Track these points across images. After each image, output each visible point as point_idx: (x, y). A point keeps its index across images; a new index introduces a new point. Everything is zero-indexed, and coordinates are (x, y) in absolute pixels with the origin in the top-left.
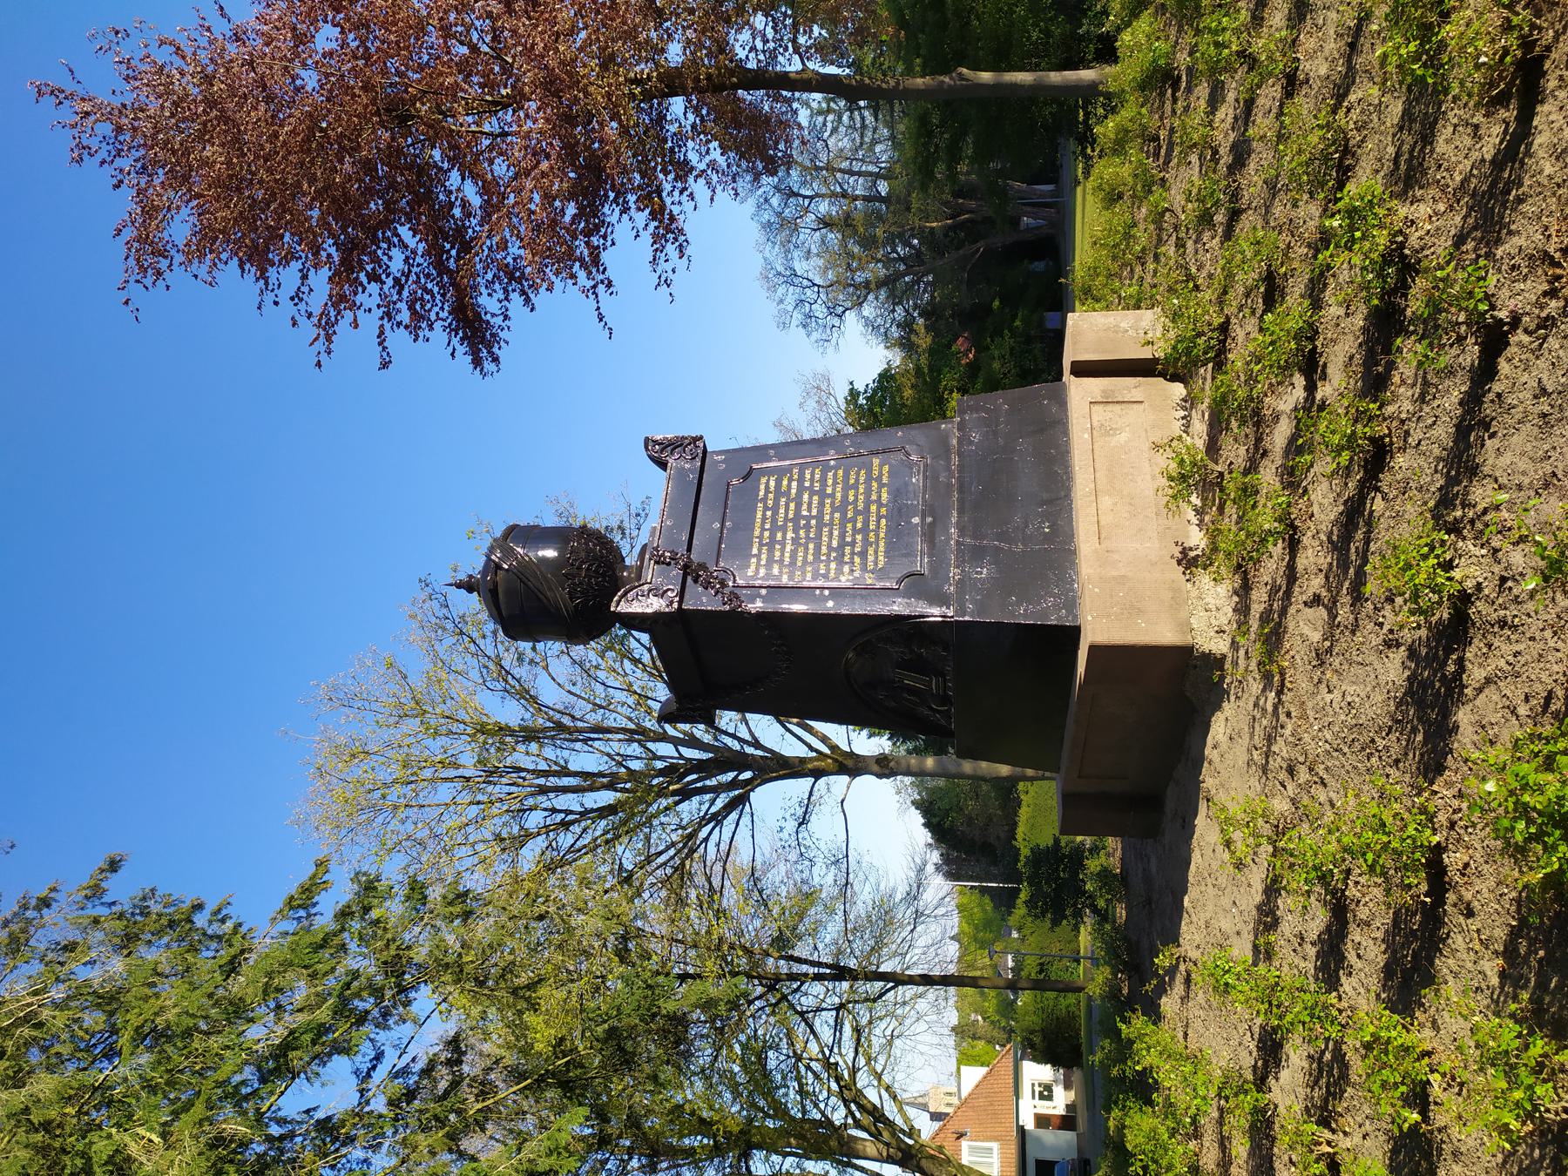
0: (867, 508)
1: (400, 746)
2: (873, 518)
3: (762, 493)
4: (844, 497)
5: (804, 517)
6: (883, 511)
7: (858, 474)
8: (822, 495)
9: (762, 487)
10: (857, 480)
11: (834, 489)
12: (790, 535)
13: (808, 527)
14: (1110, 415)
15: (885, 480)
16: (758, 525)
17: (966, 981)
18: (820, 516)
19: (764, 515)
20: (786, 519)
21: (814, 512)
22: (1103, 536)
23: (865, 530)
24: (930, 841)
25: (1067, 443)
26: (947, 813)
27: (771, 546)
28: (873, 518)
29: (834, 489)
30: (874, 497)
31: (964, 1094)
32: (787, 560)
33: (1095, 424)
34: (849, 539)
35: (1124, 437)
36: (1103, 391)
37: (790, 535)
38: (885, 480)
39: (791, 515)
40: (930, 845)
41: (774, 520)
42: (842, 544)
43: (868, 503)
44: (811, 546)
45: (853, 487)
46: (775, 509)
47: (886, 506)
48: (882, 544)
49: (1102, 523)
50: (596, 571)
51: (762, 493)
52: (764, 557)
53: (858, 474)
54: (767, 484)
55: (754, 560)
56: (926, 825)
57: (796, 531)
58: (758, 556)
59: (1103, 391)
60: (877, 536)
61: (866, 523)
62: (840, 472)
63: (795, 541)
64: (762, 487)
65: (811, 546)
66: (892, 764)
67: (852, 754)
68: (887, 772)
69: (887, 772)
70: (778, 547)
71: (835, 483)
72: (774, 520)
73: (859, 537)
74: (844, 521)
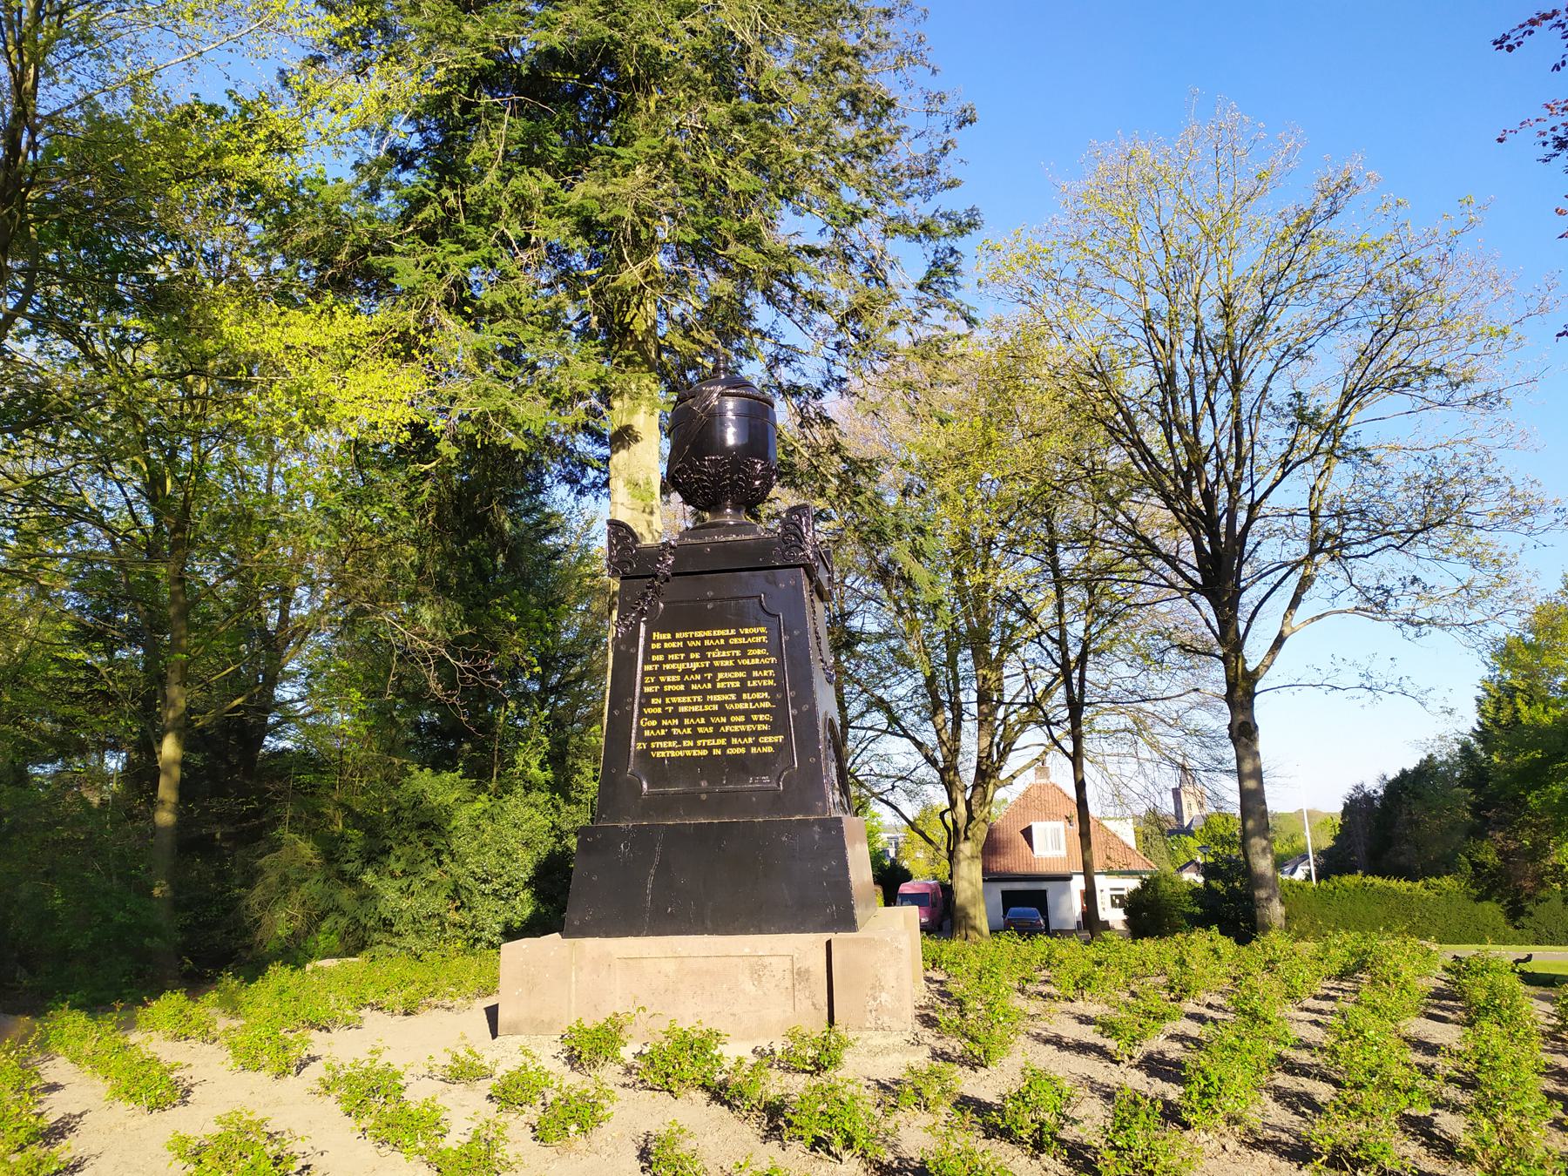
0: (723, 735)
1: (422, 400)
2: (711, 742)
3: (747, 631)
4: (738, 712)
5: (715, 676)
6: (717, 752)
7: (764, 722)
8: (744, 688)
9: (754, 630)
10: (758, 722)
11: (747, 701)
12: (695, 666)
13: (704, 681)
14: (779, 975)
15: (753, 750)
16: (708, 633)
17: (1084, 830)
18: (715, 691)
19: (719, 638)
20: (712, 659)
21: (719, 685)
22: (628, 961)
23: (695, 736)
24: (1391, 777)
25: (770, 933)
26: (1418, 796)
27: (687, 650)
28: (711, 742)
29: (747, 701)
30: (734, 741)
31: (1105, 823)
32: (667, 666)
33: (767, 961)
34: (686, 721)
35: (749, 987)
36: (807, 971)
37: (695, 666)
38: (753, 750)
39: (716, 663)
40: (1385, 778)
41: (712, 648)
42: (681, 716)
43: (729, 736)
44: (682, 687)
45: (749, 721)
46: (727, 647)
47: (724, 752)
48: (681, 753)
49: (644, 961)
50: (705, 487)
51: (747, 631)
52: (673, 645)
53: (764, 722)
54: (760, 634)
55: (669, 636)
56: (1404, 773)
57: (699, 671)
58: (674, 639)
59: (807, 971)
60: (690, 748)
61: (706, 736)
62: (767, 705)
63: (688, 672)
64: (754, 630)
65: (682, 687)
66: (1244, 739)
67: (1251, 695)
68: (1235, 735)
69: (1235, 735)
70: (683, 655)
71: (754, 701)
72: (712, 648)
73: (689, 731)
74: (707, 715)
